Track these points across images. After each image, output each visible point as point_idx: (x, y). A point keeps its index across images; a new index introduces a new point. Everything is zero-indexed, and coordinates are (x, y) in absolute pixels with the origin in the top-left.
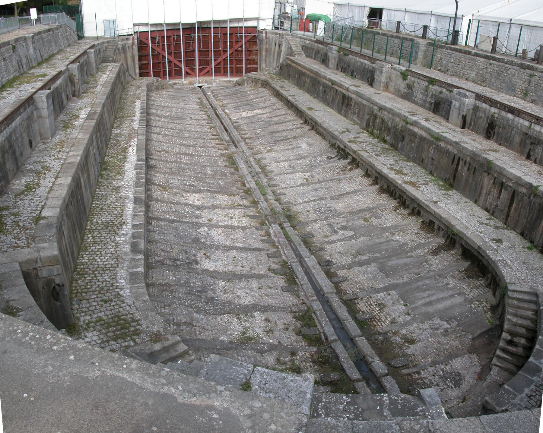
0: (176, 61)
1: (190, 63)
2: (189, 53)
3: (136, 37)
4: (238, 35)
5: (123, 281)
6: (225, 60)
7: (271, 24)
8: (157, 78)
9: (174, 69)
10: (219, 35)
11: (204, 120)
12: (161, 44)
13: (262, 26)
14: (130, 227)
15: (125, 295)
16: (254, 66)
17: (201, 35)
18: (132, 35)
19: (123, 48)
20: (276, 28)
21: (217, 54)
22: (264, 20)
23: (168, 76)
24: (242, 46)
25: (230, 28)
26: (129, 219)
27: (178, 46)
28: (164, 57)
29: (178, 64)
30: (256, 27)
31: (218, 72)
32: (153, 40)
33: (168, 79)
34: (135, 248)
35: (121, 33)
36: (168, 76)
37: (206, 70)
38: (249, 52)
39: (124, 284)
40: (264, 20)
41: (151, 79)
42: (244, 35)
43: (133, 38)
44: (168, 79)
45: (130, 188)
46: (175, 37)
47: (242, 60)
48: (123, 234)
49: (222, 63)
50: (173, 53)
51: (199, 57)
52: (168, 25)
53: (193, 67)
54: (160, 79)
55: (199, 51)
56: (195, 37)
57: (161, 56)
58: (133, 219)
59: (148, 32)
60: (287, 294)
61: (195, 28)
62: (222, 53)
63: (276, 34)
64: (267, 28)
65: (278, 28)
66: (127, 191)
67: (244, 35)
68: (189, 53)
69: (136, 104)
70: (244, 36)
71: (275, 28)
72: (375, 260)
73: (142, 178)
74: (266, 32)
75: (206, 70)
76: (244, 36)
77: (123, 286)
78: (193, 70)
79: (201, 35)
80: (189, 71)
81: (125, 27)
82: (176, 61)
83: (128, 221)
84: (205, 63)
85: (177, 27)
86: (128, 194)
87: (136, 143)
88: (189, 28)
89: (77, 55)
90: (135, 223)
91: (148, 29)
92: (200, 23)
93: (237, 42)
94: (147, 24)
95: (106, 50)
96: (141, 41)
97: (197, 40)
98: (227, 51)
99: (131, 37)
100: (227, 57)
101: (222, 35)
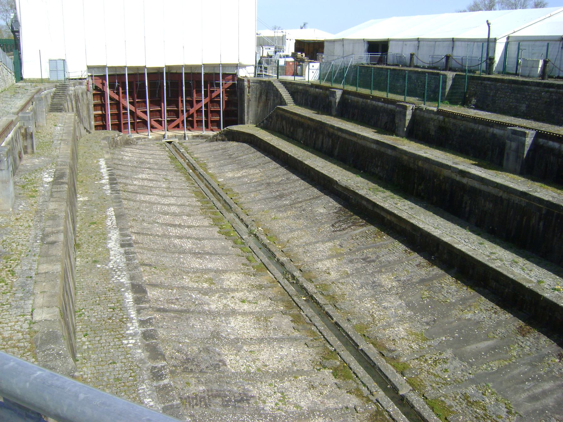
13: (242, 73)
14: (137, 324)
16: (234, 118)
18: (85, 79)
19: (75, 95)
22: (244, 66)
31: (191, 125)
35: (72, 76)
37: (175, 123)
39: (152, 404)
40: (244, 66)
41: (111, 133)
45: (122, 272)
46: (139, 83)
48: (131, 335)
51: (390, 69)
58: (139, 311)
64: (248, 76)
66: (119, 276)
71: (258, 74)
74: (249, 81)
75: (175, 123)
81: (77, 69)
83: (132, 316)
86: (122, 281)
87: (113, 213)
90: (143, 318)
92: (168, 67)
95: (59, 94)
97: (165, 87)
99: (86, 81)
100: (201, 107)
101: (195, 82)
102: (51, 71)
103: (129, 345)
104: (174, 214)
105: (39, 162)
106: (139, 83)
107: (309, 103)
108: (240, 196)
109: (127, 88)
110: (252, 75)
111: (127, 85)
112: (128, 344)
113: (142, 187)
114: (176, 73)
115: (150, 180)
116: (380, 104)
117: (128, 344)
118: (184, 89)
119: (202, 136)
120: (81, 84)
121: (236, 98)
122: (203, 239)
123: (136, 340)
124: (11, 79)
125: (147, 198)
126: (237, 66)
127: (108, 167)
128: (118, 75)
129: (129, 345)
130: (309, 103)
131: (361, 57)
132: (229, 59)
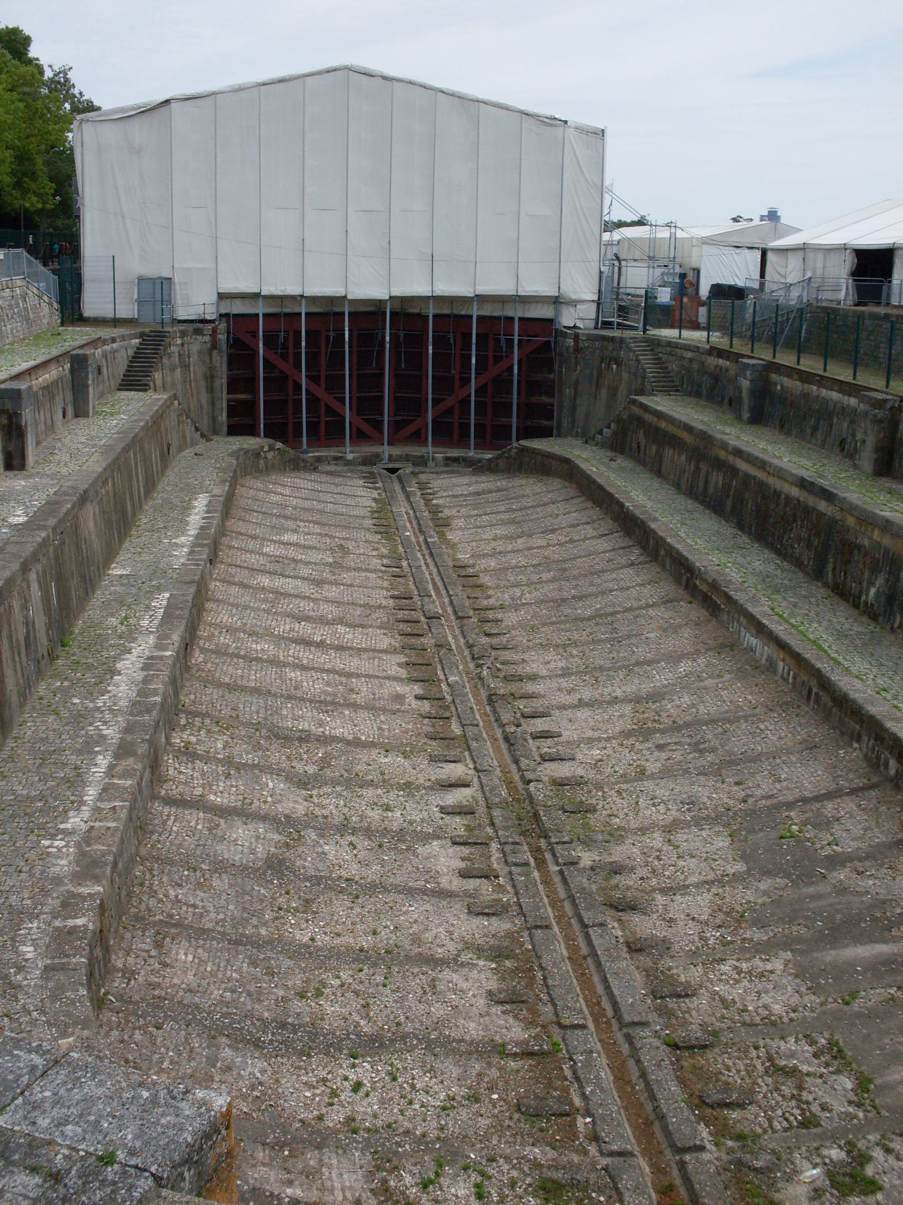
0: (327, 398)
1: (367, 406)
2: (368, 381)
3: (223, 326)
4: (502, 337)
5: (31, 949)
6: (465, 402)
7: (594, 316)
8: (271, 441)
9: (324, 419)
10: (451, 335)
11: (382, 557)
12: (291, 350)
13: (568, 318)
15: (25, 983)
17: (402, 334)
20: (607, 325)
21: (443, 384)
23: (304, 439)
24: (512, 367)
25: (480, 318)
26: (91, 793)
27: (336, 360)
28: (298, 387)
29: (336, 405)
30: (551, 321)
32: (270, 340)
33: (305, 447)
34: (87, 868)
35: (183, 313)
36: (304, 439)
38: (530, 387)
40: (574, 303)
42: (516, 338)
43: (214, 331)
44: (305, 447)
46: (332, 334)
47: (511, 404)
49: (457, 410)
50: (323, 380)
52: (314, 300)
53: (378, 418)
54: (279, 445)
55: (395, 376)
56: (384, 337)
57: (291, 383)
59: (257, 315)
60: (497, 1010)
61: (385, 313)
62: (457, 384)
63: (604, 338)
64: (580, 324)
65: (611, 323)
67: (516, 338)
68: (368, 381)
69: (196, 503)
70: (516, 342)
71: (604, 323)
72: (786, 943)
73: (155, 692)
74: (576, 337)
76: (516, 342)
77: (27, 960)
78: (378, 425)
79: (402, 334)
80: (366, 428)
81: (195, 300)
82: (327, 398)
84: (409, 406)
85: (337, 310)
88: (368, 315)
89: (32, 363)
91: (260, 309)
93: (498, 359)
94: (256, 296)
96: (236, 340)
98: (469, 380)
99: (210, 327)
100: (469, 396)
102: (140, 302)
103: (50, 850)
104: (323, 621)
105: (24, 486)
106: (332, 334)
107: (705, 392)
108: (491, 592)
109: (303, 344)
110: (591, 324)
111: (303, 338)
112: (51, 846)
113: (277, 560)
114: (419, 315)
115: (305, 547)
116: (835, 395)
117: (51, 846)
118: (430, 351)
119: (465, 459)
120: (198, 332)
121: (551, 376)
122: (358, 676)
123: (68, 842)
124: (47, 312)
125: (278, 583)
126: (557, 301)
127: (207, 512)
128: (286, 315)
129: (50, 850)
130: (705, 392)
131: (840, 288)
132: (536, 284)
